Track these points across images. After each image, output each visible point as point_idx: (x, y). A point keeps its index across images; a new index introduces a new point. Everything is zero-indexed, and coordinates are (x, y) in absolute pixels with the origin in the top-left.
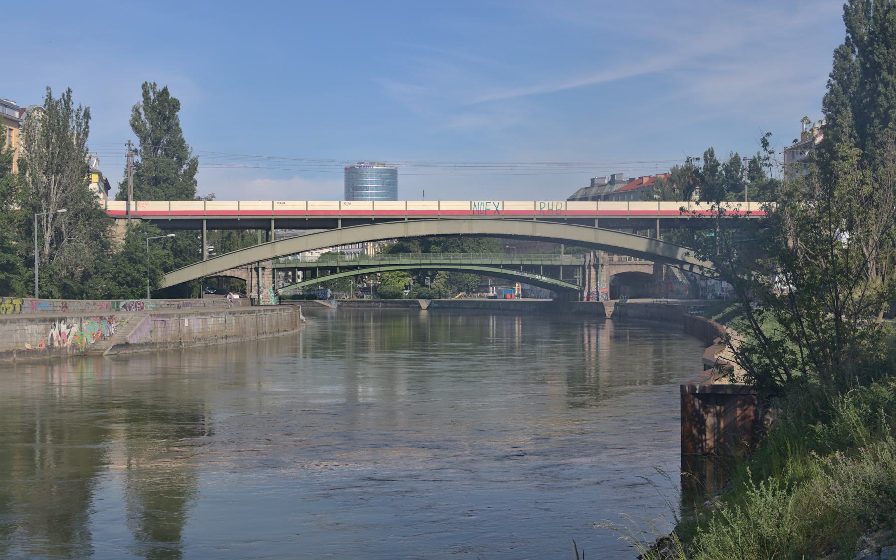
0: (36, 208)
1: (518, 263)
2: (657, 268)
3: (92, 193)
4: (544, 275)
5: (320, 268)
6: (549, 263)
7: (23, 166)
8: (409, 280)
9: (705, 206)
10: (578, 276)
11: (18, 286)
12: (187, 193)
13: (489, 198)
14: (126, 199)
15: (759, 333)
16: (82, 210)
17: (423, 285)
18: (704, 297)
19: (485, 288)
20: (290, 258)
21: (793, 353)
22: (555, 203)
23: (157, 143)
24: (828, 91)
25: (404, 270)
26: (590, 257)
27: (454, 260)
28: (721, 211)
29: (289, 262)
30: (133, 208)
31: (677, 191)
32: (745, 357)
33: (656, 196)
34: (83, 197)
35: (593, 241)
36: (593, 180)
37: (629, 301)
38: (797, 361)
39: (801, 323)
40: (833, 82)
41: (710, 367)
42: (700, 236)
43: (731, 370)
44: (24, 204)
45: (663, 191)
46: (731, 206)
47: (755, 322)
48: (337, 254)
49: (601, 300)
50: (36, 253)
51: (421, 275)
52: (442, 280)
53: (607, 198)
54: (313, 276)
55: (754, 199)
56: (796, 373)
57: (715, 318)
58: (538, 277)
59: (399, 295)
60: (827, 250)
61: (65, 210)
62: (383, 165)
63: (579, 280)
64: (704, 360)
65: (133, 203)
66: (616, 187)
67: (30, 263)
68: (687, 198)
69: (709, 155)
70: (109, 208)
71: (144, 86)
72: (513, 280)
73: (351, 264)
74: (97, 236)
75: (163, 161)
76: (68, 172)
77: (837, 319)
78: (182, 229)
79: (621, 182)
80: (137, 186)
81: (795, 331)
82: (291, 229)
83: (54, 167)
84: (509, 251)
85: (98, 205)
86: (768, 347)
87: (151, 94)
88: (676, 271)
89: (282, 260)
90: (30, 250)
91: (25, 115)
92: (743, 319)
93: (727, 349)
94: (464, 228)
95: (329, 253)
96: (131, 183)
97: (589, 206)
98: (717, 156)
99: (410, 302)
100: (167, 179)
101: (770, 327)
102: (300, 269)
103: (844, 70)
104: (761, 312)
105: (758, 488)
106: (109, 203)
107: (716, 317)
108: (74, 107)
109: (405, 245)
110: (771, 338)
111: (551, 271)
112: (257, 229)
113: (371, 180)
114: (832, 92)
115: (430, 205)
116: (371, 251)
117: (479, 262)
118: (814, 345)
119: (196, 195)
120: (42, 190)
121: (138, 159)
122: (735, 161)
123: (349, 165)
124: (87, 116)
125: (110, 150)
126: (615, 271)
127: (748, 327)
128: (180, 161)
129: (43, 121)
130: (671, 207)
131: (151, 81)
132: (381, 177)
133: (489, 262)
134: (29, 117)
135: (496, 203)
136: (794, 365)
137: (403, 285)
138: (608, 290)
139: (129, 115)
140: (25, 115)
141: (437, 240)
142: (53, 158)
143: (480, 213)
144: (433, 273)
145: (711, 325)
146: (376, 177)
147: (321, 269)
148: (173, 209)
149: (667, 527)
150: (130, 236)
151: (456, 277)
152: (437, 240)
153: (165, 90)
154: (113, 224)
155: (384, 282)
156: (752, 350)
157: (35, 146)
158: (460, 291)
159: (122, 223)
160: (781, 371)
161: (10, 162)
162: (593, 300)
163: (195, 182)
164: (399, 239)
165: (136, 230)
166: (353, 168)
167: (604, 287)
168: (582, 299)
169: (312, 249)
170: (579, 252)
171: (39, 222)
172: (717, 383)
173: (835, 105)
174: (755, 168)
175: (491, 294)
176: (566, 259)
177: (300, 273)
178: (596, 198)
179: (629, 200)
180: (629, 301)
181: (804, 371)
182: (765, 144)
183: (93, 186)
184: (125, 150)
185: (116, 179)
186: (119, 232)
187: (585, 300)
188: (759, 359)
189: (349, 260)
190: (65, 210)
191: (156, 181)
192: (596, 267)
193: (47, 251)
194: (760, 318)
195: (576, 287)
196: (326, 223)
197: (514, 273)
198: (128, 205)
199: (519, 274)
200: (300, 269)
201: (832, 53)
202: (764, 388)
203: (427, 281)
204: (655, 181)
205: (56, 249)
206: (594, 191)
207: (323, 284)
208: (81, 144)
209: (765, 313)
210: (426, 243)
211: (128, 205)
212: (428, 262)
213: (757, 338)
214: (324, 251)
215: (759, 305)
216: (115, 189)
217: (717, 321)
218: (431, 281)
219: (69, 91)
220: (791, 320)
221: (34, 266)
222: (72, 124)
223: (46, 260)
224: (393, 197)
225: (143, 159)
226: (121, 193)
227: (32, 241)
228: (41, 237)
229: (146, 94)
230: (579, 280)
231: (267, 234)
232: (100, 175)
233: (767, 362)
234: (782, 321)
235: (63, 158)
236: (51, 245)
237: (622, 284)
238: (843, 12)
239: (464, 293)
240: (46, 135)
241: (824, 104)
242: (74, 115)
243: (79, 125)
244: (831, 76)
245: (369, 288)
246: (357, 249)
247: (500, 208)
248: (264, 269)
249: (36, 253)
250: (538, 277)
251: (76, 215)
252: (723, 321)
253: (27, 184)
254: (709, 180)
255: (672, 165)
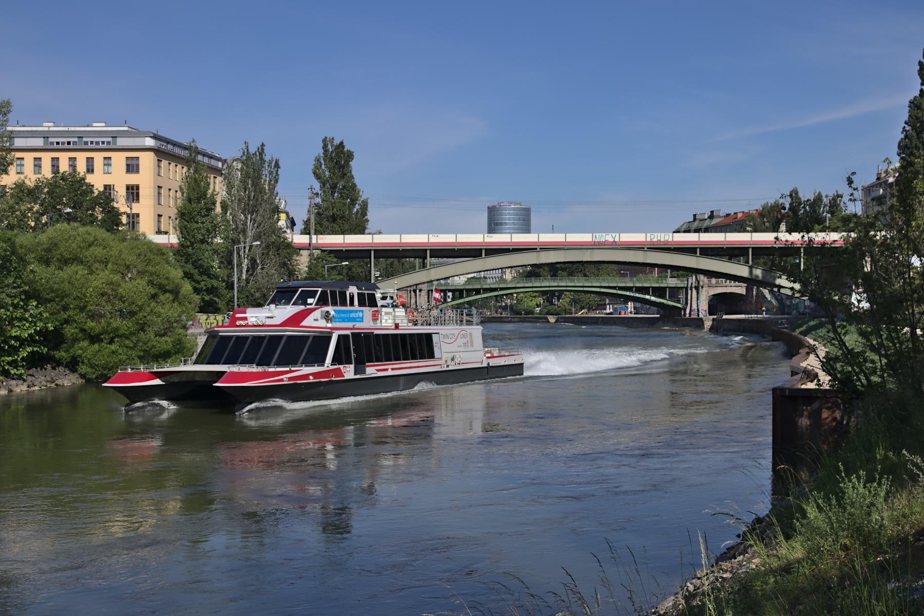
0: (235, 242)
1: (631, 285)
2: (749, 290)
3: (281, 229)
4: (655, 296)
5: (467, 290)
6: (657, 285)
7: (224, 207)
8: (540, 300)
9: (795, 237)
10: (682, 296)
11: (221, 304)
12: (360, 228)
13: (607, 231)
14: (309, 234)
15: (842, 343)
16: (273, 243)
17: (552, 304)
18: (789, 314)
19: (604, 307)
20: (442, 281)
21: (873, 362)
22: (663, 235)
23: (334, 187)
24: (903, 136)
25: (536, 292)
26: (692, 280)
27: (578, 283)
28: (810, 240)
29: (441, 285)
30: (314, 241)
31: (767, 224)
32: (830, 365)
33: (749, 229)
34: (273, 232)
35: (695, 267)
36: (695, 216)
37: (725, 317)
38: (876, 368)
39: (881, 336)
40: (908, 128)
41: (797, 374)
42: (786, 262)
43: (816, 375)
44: (225, 239)
45: (754, 224)
46: (819, 237)
47: (839, 335)
48: (480, 278)
49: (701, 316)
50: (235, 279)
51: (550, 295)
52: (568, 300)
53: (707, 230)
54: (461, 297)
55: (835, 230)
56: (875, 379)
57: (798, 331)
58: (647, 297)
59: (532, 313)
60: (905, 273)
61: (258, 243)
62: (520, 204)
63: (683, 300)
64: (791, 367)
65: (314, 237)
66: (715, 221)
67: (230, 286)
68: (775, 229)
69: (794, 195)
70: (295, 241)
71: (325, 140)
72: (627, 299)
73: (493, 286)
74: (285, 264)
75: (340, 203)
76: (261, 211)
77: (913, 333)
78: (355, 258)
79: (719, 217)
80: (319, 223)
81: (874, 342)
82: (443, 257)
83: (250, 208)
84: (624, 275)
85: (286, 239)
86: (850, 356)
87: (330, 146)
88: (766, 292)
89: (435, 283)
90: (230, 276)
91: (226, 166)
92: (828, 332)
93: (812, 356)
94: (587, 256)
95: (473, 278)
96: (313, 221)
97: (692, 237)
98: (801, 195)
99: (540, 318)
100: (343, 217)
101: (852, 340)
102: (450, 291)
103: (917, 118)
104: (844, 327)
105: (850, 481)
106: (295, 236)
107: (801, 329)
108: (267, 158)
109: (537, 270)
110: (853, 349)
111: (659, 292)
112: (415, 258)
113: (508, 216)
114: (906, 137)
115: (558, 238)
116: (508, 276)
117: (598, 285)
118: (891, 355)
119: (367, 231)
120: (241, 226)
121: (318, 200)
122: (819, 198)
123: (491, 204)
124: (277, 165)
125: (296, 196)
126: (714, 291)
127: (833, 339)
128: (353, 202)
129: (242, 170)
130: (766, 238)
131: (329, 136)
132: (517, 214)
133: (606, 285)
134: (229, 167)
135: (614, 235)
136: (874, 372)
137: (536, 304)
138: (706, 308)
139: (311, 164)
140: (226, 166)
141: (564, 266)
142: (249, 200)
143: (600, 243)
144: (560, 294)
145: (796, 338)
146: (513, 214)
147: (468, 290)
148: (346, 241)
149: (763, 507)
150: (312, 264)
151: (579, 298)
152: (564, 266)
153: (342, 143)
154: (298, 254)
155: (519, 301)
156: (836, 359)
157: (234, 191)
158: (582, 308)
159: (305, 253)
160: (862, 377)
161: (214, 203)
162: (694, 316)
163: (367, 221)
164: (532, 265)
165: (317, 259)
166: (494, 207)
167: (704, 305)
168: (685, 314)
169: (460, 274)
170: (683, 276)
171: (238, 253)
172: (803, 387)
173: (909, 148)
174: (834, 205)
175: (608, 311)
176: (672, 282)
177: (450, 294)
178: (697, 231)
179: (726, 232)
180: (725, 317)
181: (882, 376)
182: (850, 182)
183: (282, 223)
184: (308, 193)
185: (301, 216)
186: (303, 261)
187: (687, 316)
188: (842, 366)
189: (490, 283)
190: (258, 243)
191: (334, 219)
192: (697, 288)
193: (244, 276)
194: (843, 331)
195: (680, 306)
196: (473, 252)
197: (628, 293)
198: (311, 239)
199: (632, 294)
200: (450, 291)
201: (907, 104)
202: (845, 390)
203: (555, 301)
204: (748, 216)
205: (251, 275)
206: (695, 225)
207: (469, 303)
208: (272, 189)
209: (848, 327)
210: (554, 269)
211: (311, 239)
212: (572, 284)
213: (841, 349)
214: (472, 275)
215: (843, 320)
216: (300, 226)
217: (801, 333)
218: (558, 300)
219: (263, 145)
220: (871, 333)
221: (233, 289)
222: (265, 172)
223: (243, 284)
224: (528, 231)
225: (323, 201)
226: (305, 229)
227: (233, 268)
228: (240, 265)
229: (325, 147)
230: (683, 300)
231: (424, 263)
232: (287, 214)
233: (850, 369)
234: (862, 334)
235: (257, 200)
236: (247, 271)
237: (719, 303)
238: (918, 68)
239: (585, 310)
240: (243, 181)
241: (899, 147)
242: (267, 164)
243: (271, 173)
244: (906, 123)
245: (506, 305)
246: (498, 274)
247: (617, 240)
248: (420, 290)
249: (235, 279)
250: (647, 297)
251: (268, 247)
252: (805, 333)
253: (228, 221)
254: (802, 215)
255: (763, 202)
